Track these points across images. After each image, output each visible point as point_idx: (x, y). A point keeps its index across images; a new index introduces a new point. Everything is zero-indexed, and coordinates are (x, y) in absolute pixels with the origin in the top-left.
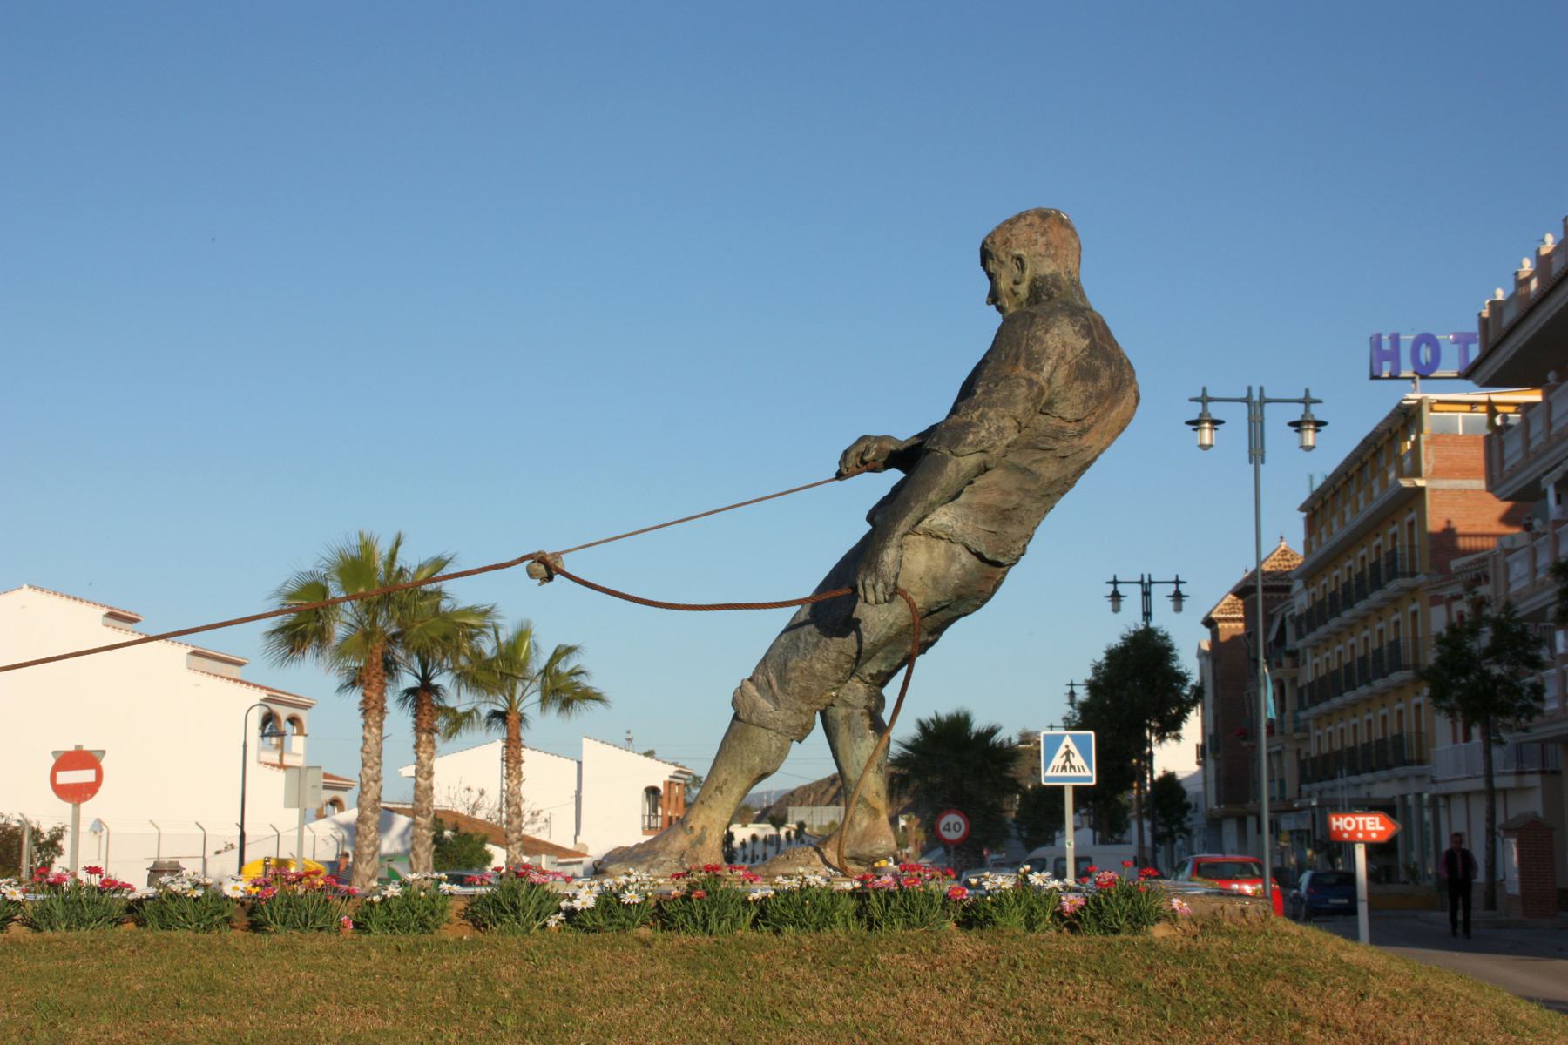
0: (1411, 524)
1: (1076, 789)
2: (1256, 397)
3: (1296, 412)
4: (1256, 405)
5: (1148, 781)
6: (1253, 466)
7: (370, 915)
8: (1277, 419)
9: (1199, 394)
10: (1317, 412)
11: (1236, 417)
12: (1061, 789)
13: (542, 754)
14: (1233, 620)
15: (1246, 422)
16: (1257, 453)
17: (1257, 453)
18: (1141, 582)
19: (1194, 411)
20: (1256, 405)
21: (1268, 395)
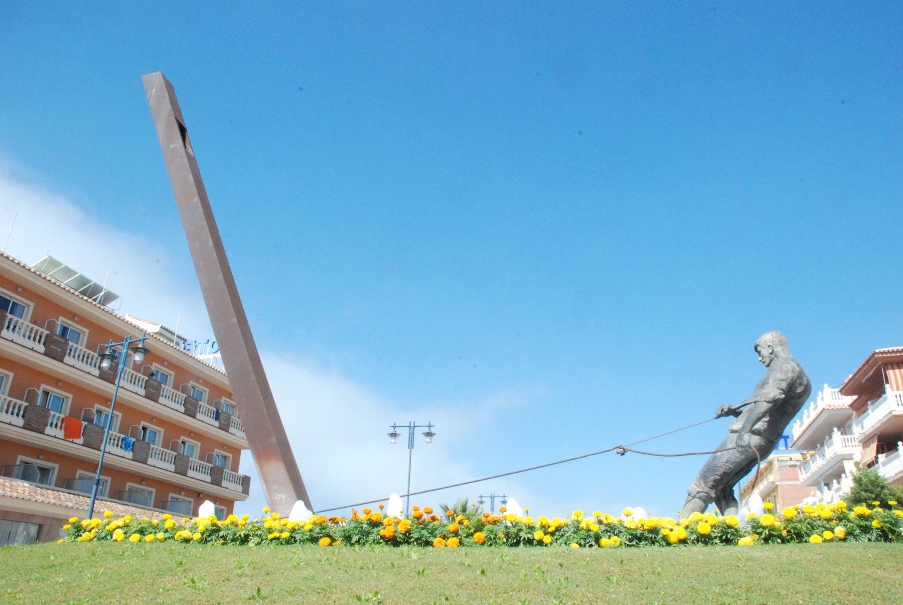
0: (775, 496)
1: (13, 302)
2: (412, 425)
3: (426, 430)
4: (412, 428)
5: (58, 339)
6: (409, 450)
7: (199, 347)
8: (419, 432)
9: (393, 425)
10: (433, 430)
11: (404, 433)
12: (10, 301)
13: (23, 262)
14: (48, 406)
15: (863, 361)
16: (411, 446)
17: (411, 446)
18: (491, 497)
19: (392, 430)
20: (412, 428)
21: (416, 425)
